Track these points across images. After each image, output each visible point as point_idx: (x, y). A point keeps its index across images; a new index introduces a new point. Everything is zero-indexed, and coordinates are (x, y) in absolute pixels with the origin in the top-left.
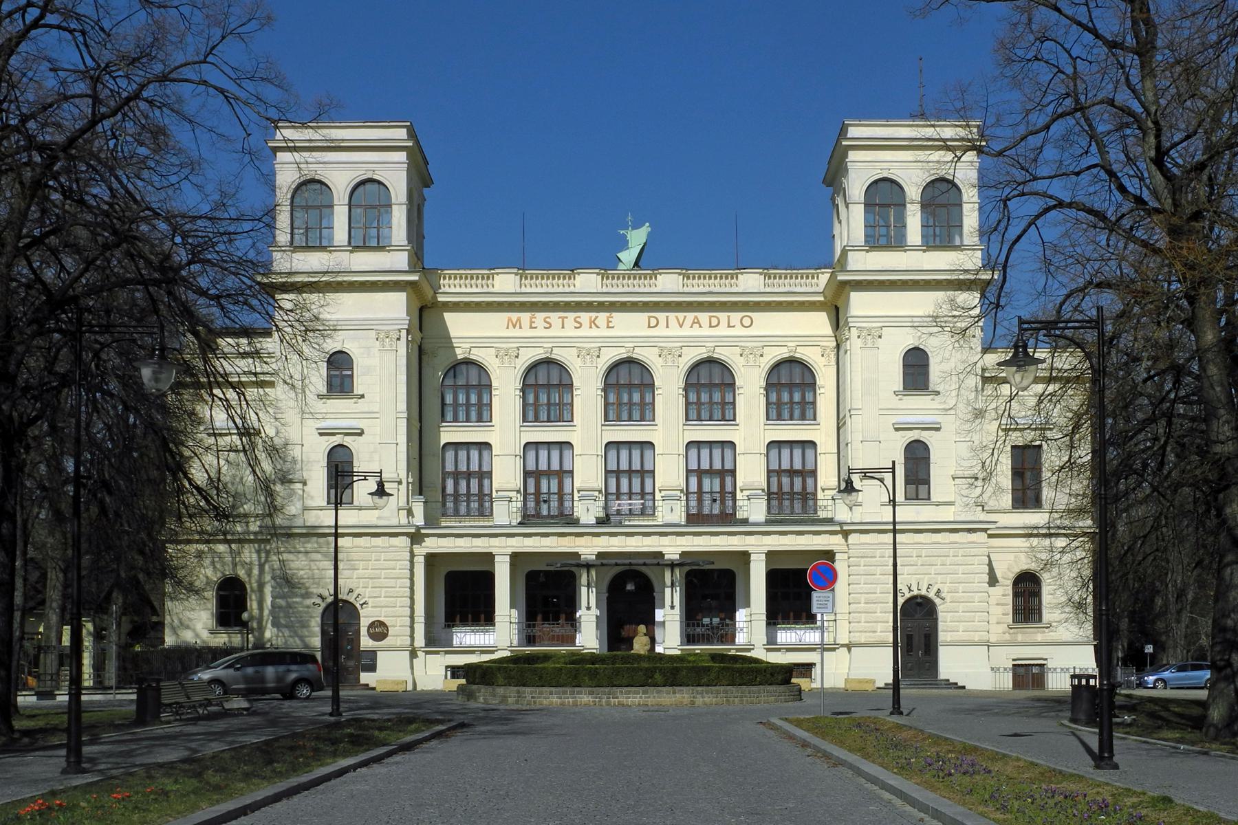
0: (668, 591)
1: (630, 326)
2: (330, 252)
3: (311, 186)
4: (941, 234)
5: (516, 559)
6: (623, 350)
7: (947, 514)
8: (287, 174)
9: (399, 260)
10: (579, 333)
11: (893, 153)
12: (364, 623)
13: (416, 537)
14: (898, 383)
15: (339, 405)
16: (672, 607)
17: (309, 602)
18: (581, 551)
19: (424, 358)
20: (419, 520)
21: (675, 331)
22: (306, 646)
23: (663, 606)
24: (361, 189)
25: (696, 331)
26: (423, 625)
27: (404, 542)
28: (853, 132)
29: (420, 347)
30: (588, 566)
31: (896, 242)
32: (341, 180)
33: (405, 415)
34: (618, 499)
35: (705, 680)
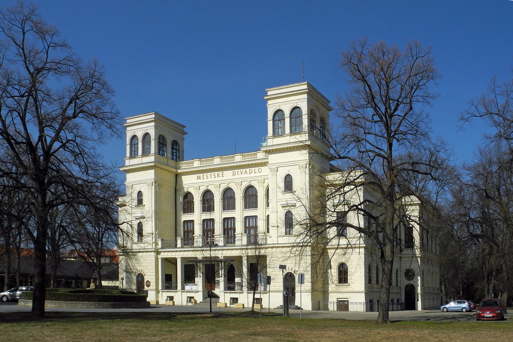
1: (228, 175)
3: (134, 137)
4: (295, 129)
5: (182, 259)
8: (272, 107)
9: (304, 138)
10: (215, 179)
11: (289, 98)
12: (145, 281)
13: (158, 253)
18: (219, 256)
19: (177, 192)
20: (160, 246)
21: (240, 176)
22: (131, 289)
24: (294, 112)
25: (246, 176)
26: (223, 283)
27: (153, 254)
28: (269, 93)
29: (175, 189)
30: (200, 261)
31: (283, 135)
32: (140, 135)
34: (341, 234)
35: (54, 298)
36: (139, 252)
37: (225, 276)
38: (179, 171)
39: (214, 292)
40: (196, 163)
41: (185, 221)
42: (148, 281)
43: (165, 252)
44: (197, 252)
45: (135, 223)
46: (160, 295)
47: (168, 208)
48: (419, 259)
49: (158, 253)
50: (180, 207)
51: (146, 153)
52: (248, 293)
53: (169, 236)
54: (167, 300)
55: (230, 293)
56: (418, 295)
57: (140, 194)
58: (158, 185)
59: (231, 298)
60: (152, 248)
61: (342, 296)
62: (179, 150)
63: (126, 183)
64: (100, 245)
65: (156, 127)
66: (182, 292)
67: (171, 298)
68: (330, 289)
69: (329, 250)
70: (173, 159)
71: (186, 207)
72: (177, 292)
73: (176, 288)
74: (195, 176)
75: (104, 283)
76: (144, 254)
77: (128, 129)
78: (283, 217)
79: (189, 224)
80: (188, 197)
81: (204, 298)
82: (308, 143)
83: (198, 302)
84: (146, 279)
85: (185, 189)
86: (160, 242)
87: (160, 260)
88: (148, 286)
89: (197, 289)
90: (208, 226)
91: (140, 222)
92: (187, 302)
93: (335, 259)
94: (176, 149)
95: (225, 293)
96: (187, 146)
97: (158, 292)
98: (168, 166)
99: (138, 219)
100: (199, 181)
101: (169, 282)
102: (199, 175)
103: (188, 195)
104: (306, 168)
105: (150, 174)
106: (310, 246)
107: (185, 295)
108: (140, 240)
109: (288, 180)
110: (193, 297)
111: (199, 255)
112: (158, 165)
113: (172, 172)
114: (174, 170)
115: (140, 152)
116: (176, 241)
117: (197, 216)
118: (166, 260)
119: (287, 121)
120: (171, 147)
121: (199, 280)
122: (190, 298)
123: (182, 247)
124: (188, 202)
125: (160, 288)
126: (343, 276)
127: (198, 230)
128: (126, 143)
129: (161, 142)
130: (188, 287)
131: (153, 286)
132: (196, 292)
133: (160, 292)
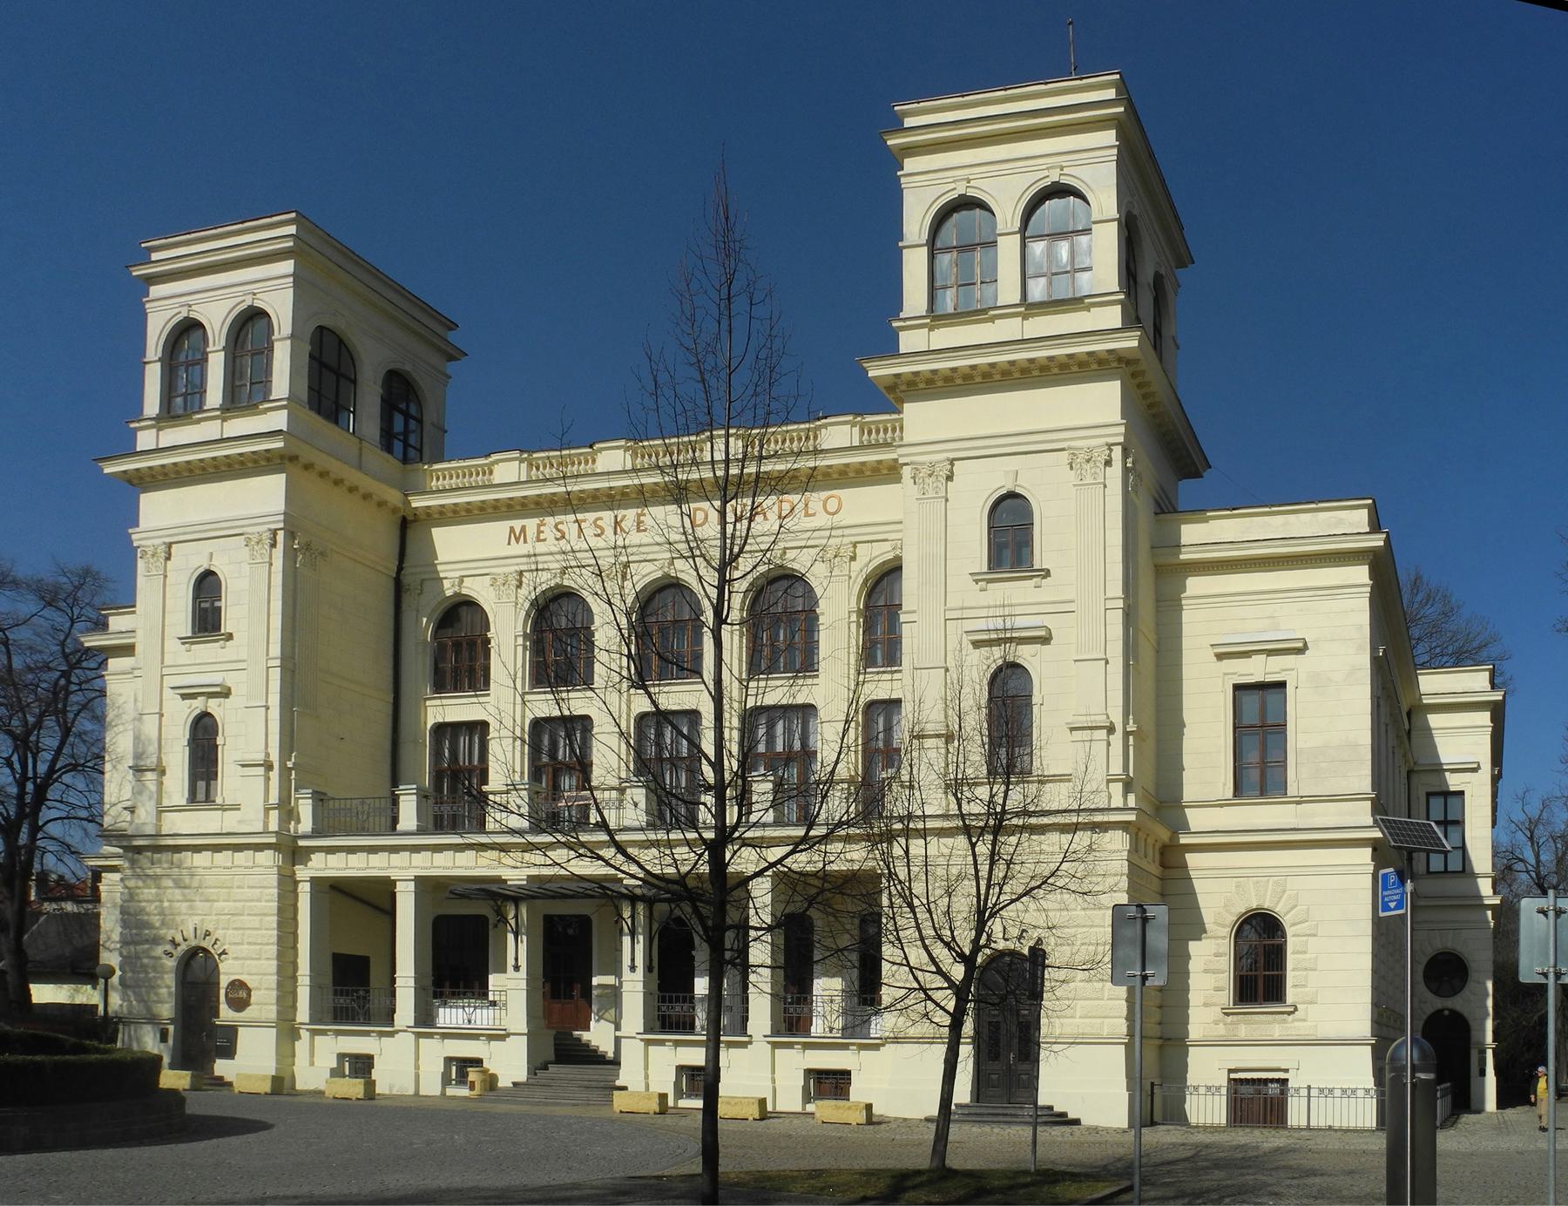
0: (626, 940)
2: (992, 319)
3: (188, 329)
5: (427, 887)
6: (887, 546)
7: (230, 822)
8: (923, 191)
12: (224, 982)
13: (293, 853)
14: (980, 561)
15: (207, 651)
16: (517, 968)
17: (159, 951)
18: (506, 873)
19: (407, 600)
20: (306, 825)
23: (502, 969)
30: (517, 897)
32: (216, 317)
33: (1120, 604)
36: (197, 849)
37: (649, 969)
38: (418, 502)
39: (585, 1036)
40: (508, 469)
41: (441, 729)
42: (237, 985)
43: (331, 850)
44: (504, 855)
45: (180, 716)
46: (302, 1047)
47: (357, 657)
48: (1489, 913)
49: (293, 853)
50: (418, 665)
51: (245, 391)
52: (775, 1045)
53: (358, 773)
54: (336, 1073)
55: (677, 1043)
56: (1483, 1052)
57: (207, 585)
58: (307, 547)
59: (809, 1073)
60: (266, 832)
61: (1255, 1060)
62: (420, 422)
63: (137, 538)
64: (23, 838)
65: (300, 282)
66: (419, 1035)
67: (362, 1065)
68: (1195, 1031)
69: (1192, 859)
70: (388, 448)
71: (448, 666)
72: (391, 1034)
73: (389, 1015)
74: (500, 529)
75: (43, 993)
76: (223, 858)
77: (156, 291)
78: (975, 695)
79: (463, 741)
80: (461, 628)
81: (537, 1066)
82: (1130, 342)
83: (504, 1082)
84: (228, 972)
85: (446, 584)
86: (305, 809)
87: (304, 889)
88: (240, 1004)
89: (499, 1026)
90: (558, 751)
91: (205, 715)
92: (446, 1080)
93: (1222, 891)
94: (407, 416)
95: (648, 1043)
96: (455, 396)
97: (287, 1031)
98: (360, 467)
99: (193, 696)
100: (522, 548)
101: (352, 988)
102: (517, 524)
103: (464, 611)
104: (1108, 463)
105: (266, 496)
106: (1124, 826)
107: (435, 1053)
108: (201, 796)
109: (1005, 519)
110: (477, 1062)
111: (514, 871)
112: (307, 454)
113: (381, 504)
114: (393, 496)
115: (214, 394)
116: (395, 802)
117: (506, 704)
118: (333, 891)
119: (1008, 248)
120: (380, 396)
121: (511, 985)
122: (462, 1067)
123: (421, 831)
124: (457, 645)
125: (303, 1013)
126: (1261, 967)
127: (506, 763)
128: (143, 353)
129: (329, 376)
130: (450, 1016)
131: (264, 1003)
132: (491, 1038)
133: (305, 1034)
